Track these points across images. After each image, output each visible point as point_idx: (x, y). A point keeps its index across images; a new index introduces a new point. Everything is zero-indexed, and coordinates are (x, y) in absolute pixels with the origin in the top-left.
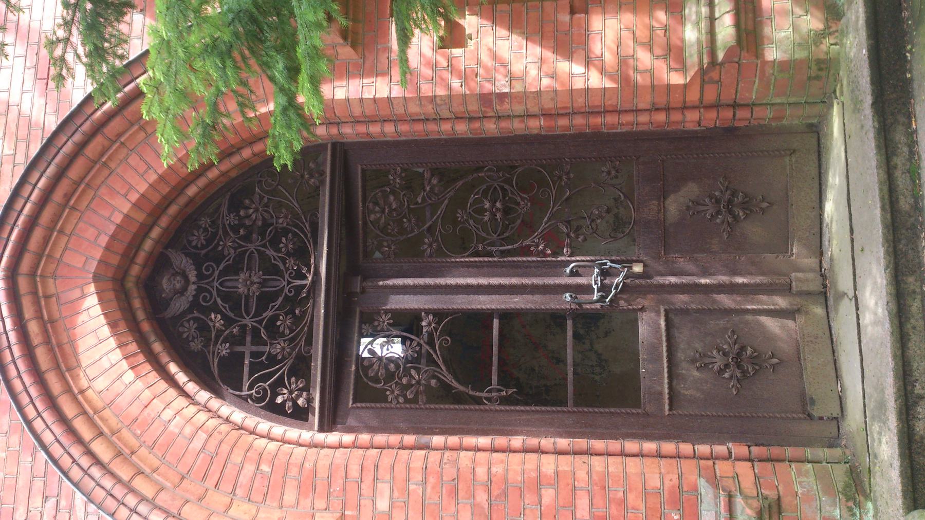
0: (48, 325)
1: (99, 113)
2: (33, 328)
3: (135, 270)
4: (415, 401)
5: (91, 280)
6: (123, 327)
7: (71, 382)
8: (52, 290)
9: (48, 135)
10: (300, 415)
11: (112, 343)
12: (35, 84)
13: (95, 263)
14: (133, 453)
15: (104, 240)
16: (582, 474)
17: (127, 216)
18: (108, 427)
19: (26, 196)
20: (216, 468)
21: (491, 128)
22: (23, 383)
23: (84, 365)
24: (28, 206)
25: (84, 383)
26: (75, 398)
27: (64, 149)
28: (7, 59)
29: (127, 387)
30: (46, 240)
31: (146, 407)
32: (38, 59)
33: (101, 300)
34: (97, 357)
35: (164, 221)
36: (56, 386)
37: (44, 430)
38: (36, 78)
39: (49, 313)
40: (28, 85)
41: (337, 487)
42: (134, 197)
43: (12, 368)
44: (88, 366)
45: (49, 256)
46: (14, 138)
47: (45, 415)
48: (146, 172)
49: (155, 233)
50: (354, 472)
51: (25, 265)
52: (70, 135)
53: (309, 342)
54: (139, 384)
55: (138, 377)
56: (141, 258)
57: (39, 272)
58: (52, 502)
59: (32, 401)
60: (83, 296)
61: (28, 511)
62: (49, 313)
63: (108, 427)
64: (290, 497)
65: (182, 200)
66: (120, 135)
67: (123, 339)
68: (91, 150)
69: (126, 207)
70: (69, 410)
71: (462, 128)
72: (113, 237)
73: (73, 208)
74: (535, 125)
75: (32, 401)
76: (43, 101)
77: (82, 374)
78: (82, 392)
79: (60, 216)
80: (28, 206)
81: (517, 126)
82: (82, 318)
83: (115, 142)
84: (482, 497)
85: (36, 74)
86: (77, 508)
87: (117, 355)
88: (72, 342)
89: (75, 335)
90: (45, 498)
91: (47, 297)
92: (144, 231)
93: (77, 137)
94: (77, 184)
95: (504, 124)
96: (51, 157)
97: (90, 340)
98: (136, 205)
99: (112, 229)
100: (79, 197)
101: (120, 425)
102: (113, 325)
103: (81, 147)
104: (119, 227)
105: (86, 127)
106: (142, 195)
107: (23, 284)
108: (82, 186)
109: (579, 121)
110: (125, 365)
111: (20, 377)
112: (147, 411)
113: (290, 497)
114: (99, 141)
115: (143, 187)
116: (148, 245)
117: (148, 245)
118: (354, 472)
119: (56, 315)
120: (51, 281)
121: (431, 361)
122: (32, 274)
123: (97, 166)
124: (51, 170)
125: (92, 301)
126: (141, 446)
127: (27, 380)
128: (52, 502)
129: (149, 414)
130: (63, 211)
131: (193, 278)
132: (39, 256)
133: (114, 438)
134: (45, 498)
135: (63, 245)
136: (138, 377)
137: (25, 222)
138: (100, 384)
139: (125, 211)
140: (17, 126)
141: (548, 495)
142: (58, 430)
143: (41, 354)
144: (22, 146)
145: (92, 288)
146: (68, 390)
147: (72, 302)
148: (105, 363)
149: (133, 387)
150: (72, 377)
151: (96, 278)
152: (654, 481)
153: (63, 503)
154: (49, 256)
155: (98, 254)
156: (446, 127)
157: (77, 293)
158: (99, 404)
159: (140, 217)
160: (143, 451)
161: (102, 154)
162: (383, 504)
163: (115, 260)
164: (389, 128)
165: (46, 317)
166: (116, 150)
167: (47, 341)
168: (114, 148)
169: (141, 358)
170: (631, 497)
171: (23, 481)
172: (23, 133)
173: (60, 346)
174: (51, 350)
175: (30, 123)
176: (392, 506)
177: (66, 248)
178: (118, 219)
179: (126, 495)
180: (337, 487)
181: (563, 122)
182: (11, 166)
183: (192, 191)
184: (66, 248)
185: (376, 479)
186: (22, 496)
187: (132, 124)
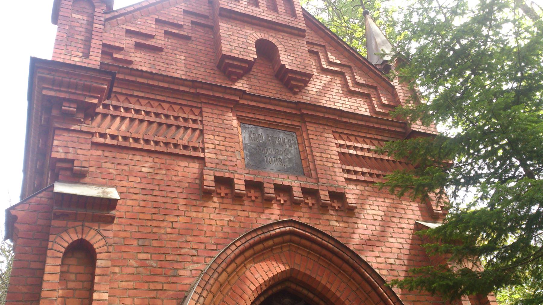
0: (271, 249)
1: (363, 270)
2: (270, 243)
3: (294, 286)
5: (291, 267)
6: (272, 282)
7: (249, 260)
8: (284, 249)
9: (347, 245)
11: (266, 278)
12: (363, 239)
13: (298, 269)
14: (221, 292)
15: (308, 272)
17: (319, 282)
18: (231, 279)
19: (324, 239)
22: (250, 240)
23: (255, 265)
24: (320, 240)
25: (248, 266)
26: (243, 262)
27: (345, 255)
29: (248, 286)
30: (305, 247)
31: (241, 297)
32: (373, 240)
33: (282, 272)
34: (259, 272)
36: (247, 254)
37: (231, 250)
38: (366, 240)
39: (275, 249)
40: (362, 236)
42: (328, 286)
43: (256, 235)
44: (255, 267)
45: (298, 248)
46: (340, 231)
47: (238, 250)
48: (340, 291)
49: (311, 295)
52: (352, 257)
54: (250, 293)
55: (253, 291)
57: (291, 244)
58: (195, 253)
59: (243, 244)
60: (283, 264)
61: (190, 242)
62: (275, 249)
63: (231, 279)
66: (353, 279)
67: (267, 284)
69: (323, 282)
70: (238, 261)
72: (310, 277)
73: (319, 258)
75: (243, 244)
76: (358, 243)
77: (251, 265)
78: (245, 265)
79: (315, 253)
80: (320, 240)
82: (275, 264)
83: (350, 277)
85: (367, 240)
86: (193, 265)
87: (262, 281)
88: (264, 260)
89: (267, 261)
90: (196, 250)
91: (281, 248)
92: (311, 290)
93: (351, 261)
94: (330, 260)
96: (341, 249)
97: (266, 268)
98: (325, 287)
99: (314, 276)
100: (324, 261)
101: (232, 284)
102: (273, 278)
104: (315, 279)
105: (356, 265)
106: (330, 290)
107: (287, 237)
108: (329, 262)
110: (258, 285)
111: (252, 238)
112: (238, 296)
114: (350, 270)
115: (333, 290)
116: (305, 292)
117: (305, 292)
119: (275, 252)
120: (288, 249)
122: (291, 241)
123: (338, 269)
125: (282, 268)
126: (223, 295)
127: (251, 241)
128: (195, 253)
129: (237, 298)
130: (318, 254)
132: (299, 244)
133: (227, 282)
134: (196, 250)
135: (303, 254)
136: (253, 291)
137: (313, 238)
138: (248, 274)
139: (322, 282)
140: (346, 232)
142: (232, 256)
143: (261, 246)
144: (338, 234)
145: (288, 268)
146: (246, 259)
147: (280, 259)
148: (257, 276)
149: (248, 290)
150: (251, 260)
151: (291, 269)
153: (195, 258)
154: (298, 248)
155: (302, 270)
157: (284, 261)
158: (240, 274)
159: (319, 289)
160: (221, 297)
161: (344, 271)
163: (299, 277)
165: (274, 248)
166: (346, 277)
167: (265, 249)
168: (348, 276)
169: (260, 292)
171: (204, 239)
172: (344, 235)
173: (263, 254)
174: (262, 250)
175: (348, 238)
177: (302, 255)
178: (318, 279)
179: (207, 291)
182: (330, 230)
184: (302, 255)
186: (196, 239)
187: (359, 284)
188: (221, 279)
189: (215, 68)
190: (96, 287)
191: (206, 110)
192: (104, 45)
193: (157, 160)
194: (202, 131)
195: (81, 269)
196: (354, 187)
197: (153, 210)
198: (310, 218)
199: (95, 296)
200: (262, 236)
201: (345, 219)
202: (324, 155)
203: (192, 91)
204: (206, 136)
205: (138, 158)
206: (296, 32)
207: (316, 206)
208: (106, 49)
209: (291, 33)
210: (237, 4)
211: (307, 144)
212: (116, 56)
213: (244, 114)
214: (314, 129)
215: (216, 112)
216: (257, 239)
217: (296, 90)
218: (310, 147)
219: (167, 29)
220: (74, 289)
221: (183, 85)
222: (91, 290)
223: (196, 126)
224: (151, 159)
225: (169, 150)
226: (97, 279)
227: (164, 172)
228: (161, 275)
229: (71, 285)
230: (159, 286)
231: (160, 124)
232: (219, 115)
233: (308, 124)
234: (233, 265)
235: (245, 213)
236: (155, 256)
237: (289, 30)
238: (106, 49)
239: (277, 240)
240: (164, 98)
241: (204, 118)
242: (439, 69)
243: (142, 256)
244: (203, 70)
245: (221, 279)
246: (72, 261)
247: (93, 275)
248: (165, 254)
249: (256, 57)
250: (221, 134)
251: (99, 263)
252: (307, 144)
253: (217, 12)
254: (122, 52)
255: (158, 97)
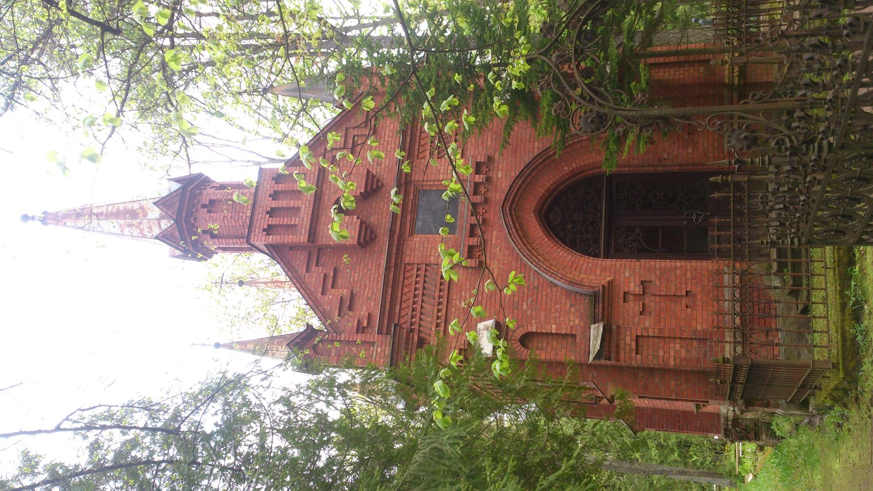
4: (634, 252)
10: (597, 256)
11: (540, 230)
15: (536, 201)
16: (689, 266)
20: (574, 266)
21: (661, 169)
28: (64, 172)
35: (552, 196)
41: (613, 270)
42: (546, 188)
49: (549, 200)
50: (618, 266)
51: (514, 206)
53: (599, 234)
56: (545, 208)
64: (598, 273)
65: (558, 190)
68: (533, 174)
69: (543, 191)
71: (651, 169)
74: (676, 169)
81: (669, 169)
84: (658, 273)
92: (548, 198)
93: (530, 170)
95: (665, 168)
97: (533, 229)
99: (539, 197)
103: (531, 172)
107: (513, 212)
109: (690, 167)
113: (598, 273)
114: (536, 171)
118: (618, 266)
121: (638, 241)
122: (515, 210)
124: (522, 179)
127: (518, 238)
131: (560, 215)
141: (678, 272)
143: (520, 232)
151: (534, 212)
152: (711, 268)
156: (646, 169)
162: (627, 275)
164: (627, 169)
170: (704, 272)
176: (630, 275)
178: (541, 195)
180: (613, 270)
181: (685, 167)
183: (561, 187)
185: (625, 268)
188: (542, 260)
189: (364, 250)
190: (549, 332)
191: (407, 260)
192: (357, 332)
193: (454, 297)
194: (427, 265)
195: (535, 341)
196: (469, 151)
197: (493, 300)
198: (496, 192)
199: (554, 332)
200: (514, 231)
201: (496, 165)
202: (442, 171)
203: (393, 270)
204: (432, 261)
205: (453, 310)
206: (321, 176)
207: (487, 186)
208: (361, 331)
209: (323, 181)
210: (300, 227)
211: (432, 183)
212: (365, 324)
213: (407, 231)
214: (417, 175)
215: (408, 253)
216: (516, 235)
217: (380, 185)
218: (434, 181)
219: (330, 286)
220: (547, 343)
221: (388, 276)
222: (552, 334)
223: (423, 269)
224: (454, 302)
225: (446, 289)
226: (544, 331)
227: (463, 293)
228: (537, 296)
229: (545, 345)
230: (544, 297)
231: (423, 294)
232: (411, 251)
233: (413, 179)
234: (533, 251)
235: (494, 239)
236: (525, 299)
237: (320, 183)
238: (361, 331)
239: (515, 220)
240: (400, 291)
241: (416, 262)
242: (472, 86)
243: (525, 307)
244: (367, 260)
245: (542, 260)
246: (530, 345)
247: (542, 334)
248: (523, 293)
249: (355, 217)
250: (429, 250)
251: (534, 330)
252: (432, 183)
253: (310, 244)
254: (361, 321)
255: (399, 295)
